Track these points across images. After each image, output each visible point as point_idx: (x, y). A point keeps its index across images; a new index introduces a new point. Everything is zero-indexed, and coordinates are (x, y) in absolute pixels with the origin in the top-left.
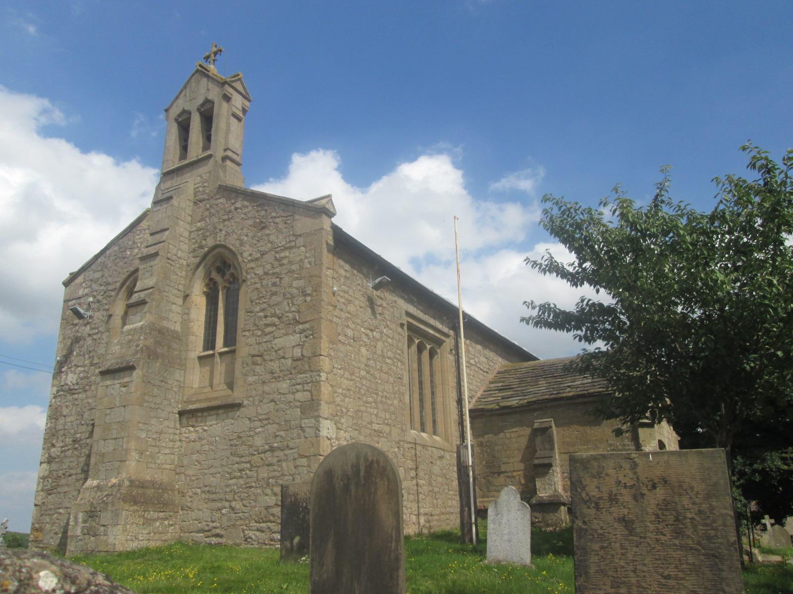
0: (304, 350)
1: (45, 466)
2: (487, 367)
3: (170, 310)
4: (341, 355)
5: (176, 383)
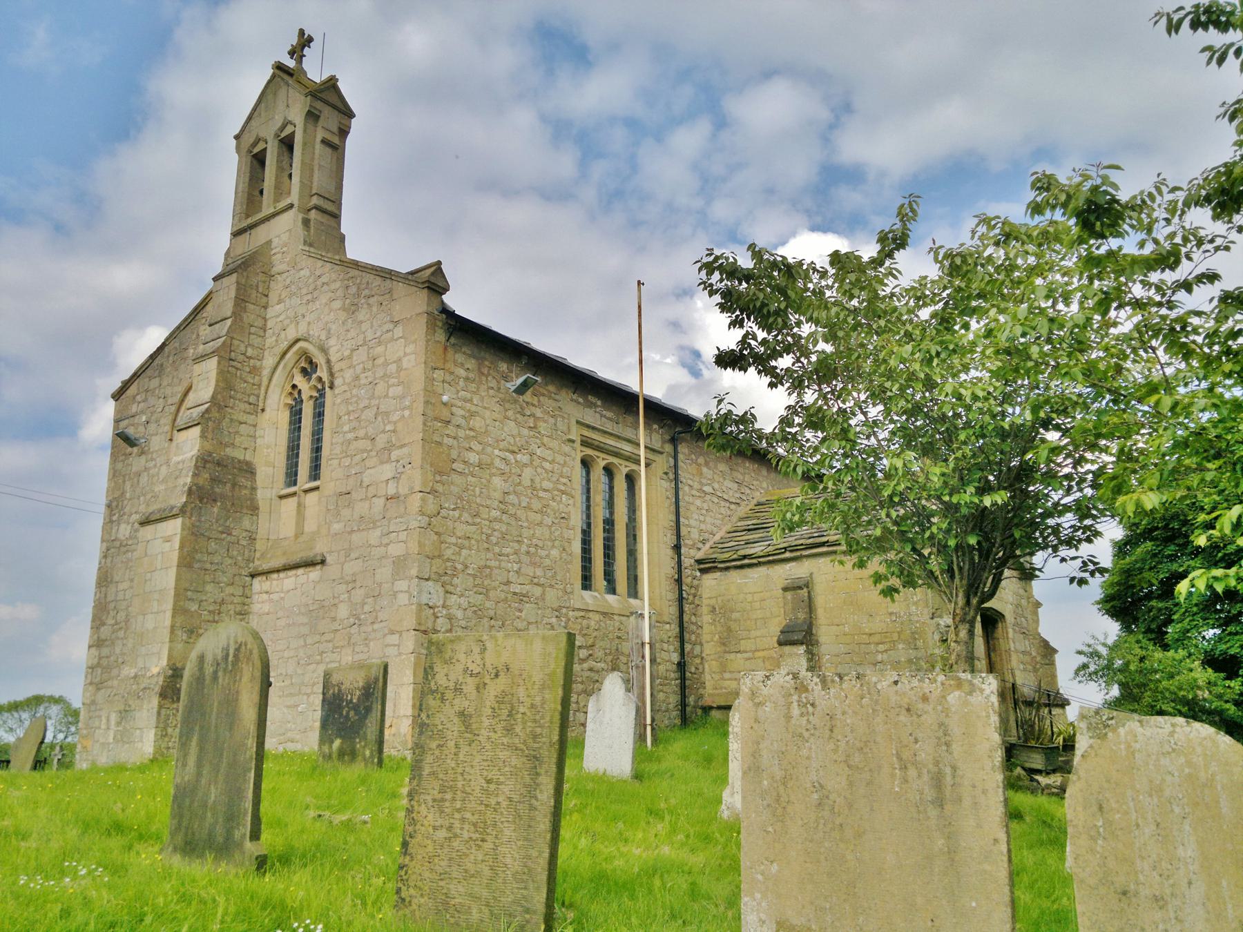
0: (400, 486)
1: (93, 650)
2: (738, 495)
3: (237, 432)
4: (455, 489)
5: (244, 534)
